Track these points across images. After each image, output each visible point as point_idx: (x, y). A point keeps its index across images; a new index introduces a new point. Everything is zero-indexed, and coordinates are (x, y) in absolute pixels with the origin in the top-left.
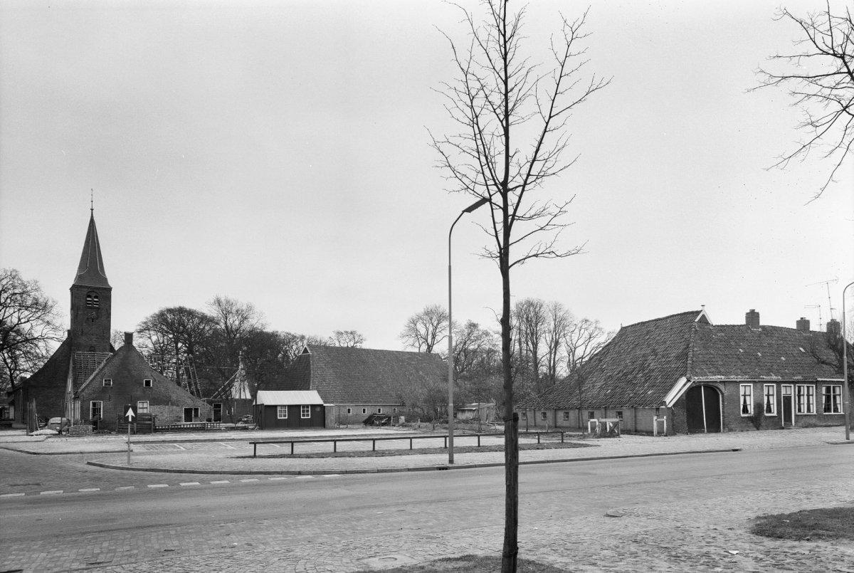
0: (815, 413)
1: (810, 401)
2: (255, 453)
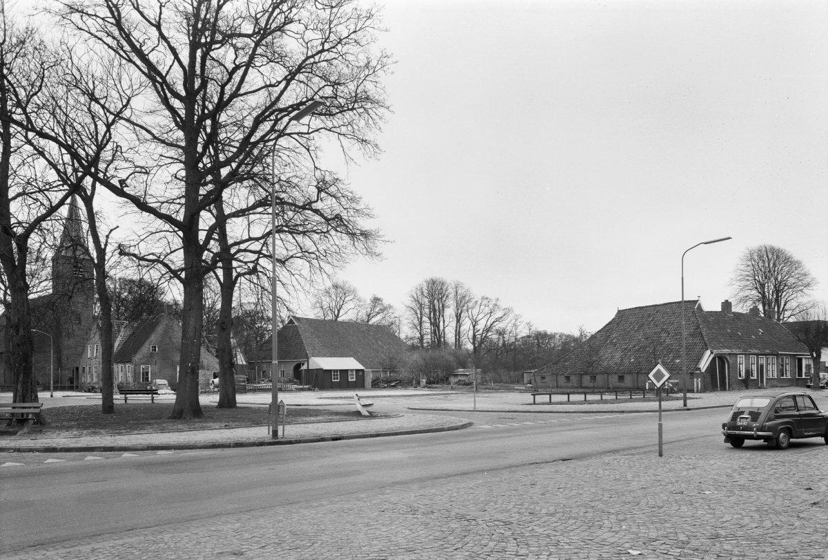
0: (776, 377)
1: (772, 371)
2: (550, 397)
